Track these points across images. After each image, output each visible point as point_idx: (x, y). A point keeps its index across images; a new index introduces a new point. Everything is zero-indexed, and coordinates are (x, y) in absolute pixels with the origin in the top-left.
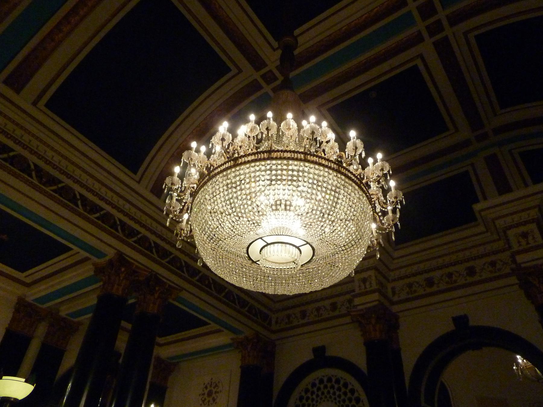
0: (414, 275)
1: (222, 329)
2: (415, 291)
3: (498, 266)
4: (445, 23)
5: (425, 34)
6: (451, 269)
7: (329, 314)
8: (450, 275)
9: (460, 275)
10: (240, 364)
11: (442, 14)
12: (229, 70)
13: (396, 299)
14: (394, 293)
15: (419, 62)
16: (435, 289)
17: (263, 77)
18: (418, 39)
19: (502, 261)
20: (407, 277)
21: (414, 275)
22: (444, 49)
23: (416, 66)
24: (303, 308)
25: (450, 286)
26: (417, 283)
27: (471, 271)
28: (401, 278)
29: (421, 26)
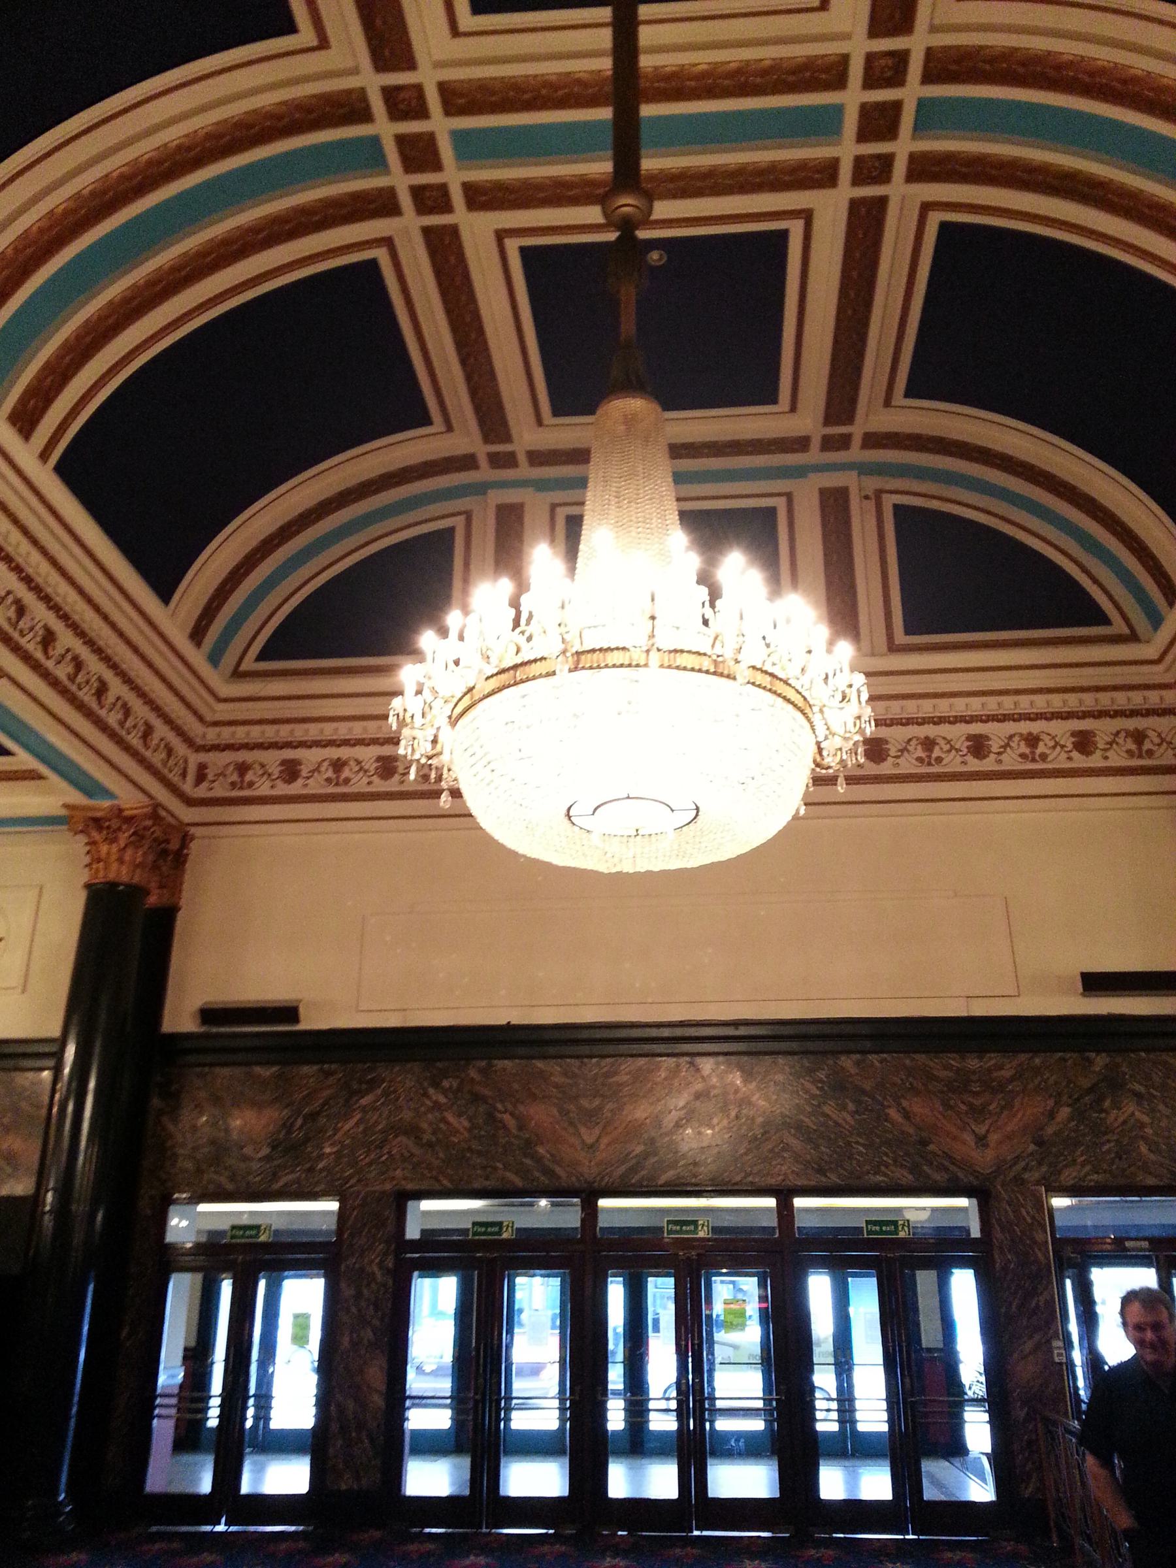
0: (940, 721)
1: (43, 770)
2: (251, 784)
3: (1041, 748)
4: (900, 168)
5: (846, 172)
6: (343, 753)
7: (1070, 759)
8: (1032, 740)
9: (361, 769)
10: (85, 877)
11: (903, 147)
12: (290, 28)
13: (201, 792)
14: (201, 777)
15: (796, 228)
16: (296, 788)
17: (390, 94)
18: (382, 204)
19: (949, 742)
20: (1133, 713)
21: (940, 721)
22: (866, 222)
23: (373, 264)
24: (289, 754)
25: (331, 790)
26: (358, 762)
27: (978, 747)
28: (908, 722)
29: (847, 149)
